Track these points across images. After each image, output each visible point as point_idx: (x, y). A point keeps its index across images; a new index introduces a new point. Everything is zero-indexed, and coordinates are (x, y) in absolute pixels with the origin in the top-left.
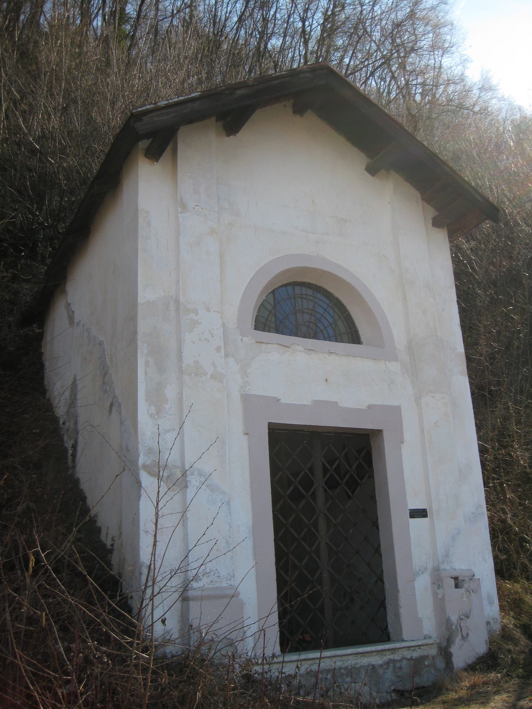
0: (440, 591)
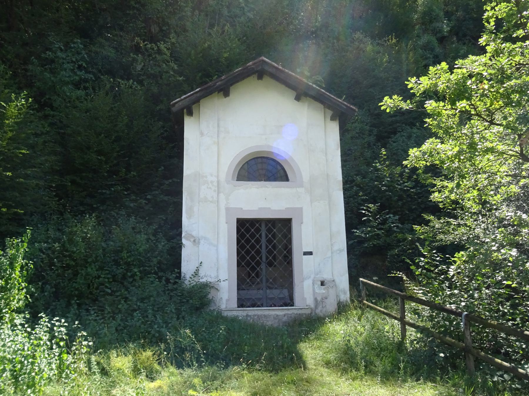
0: (192, 240)
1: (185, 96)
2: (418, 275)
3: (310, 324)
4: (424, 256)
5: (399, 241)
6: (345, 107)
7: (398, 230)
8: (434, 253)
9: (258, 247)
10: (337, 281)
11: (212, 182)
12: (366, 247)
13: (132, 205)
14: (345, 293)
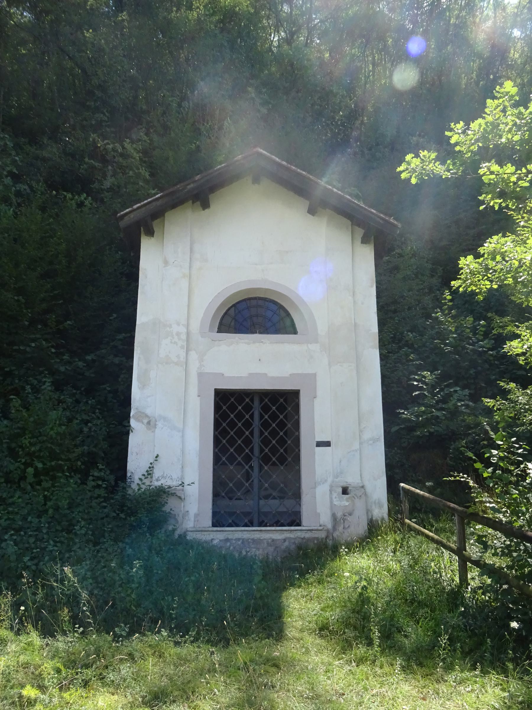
0: (145, 421)
1: (139, 205)
2: (486, 478)
3: (313, 557)
4: (498, 447)
5: (469, 427)
6: (381, 221)
7: (468, 411)
8: (513, 442)
9: (247, 433)
10: (369, 488)
11: (178, 334)
12: (418, 436)
13: (62, 369)
14: (381, 506)
